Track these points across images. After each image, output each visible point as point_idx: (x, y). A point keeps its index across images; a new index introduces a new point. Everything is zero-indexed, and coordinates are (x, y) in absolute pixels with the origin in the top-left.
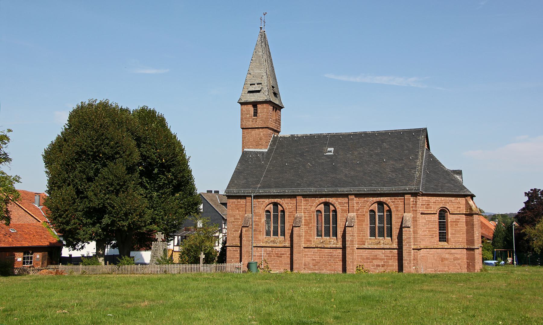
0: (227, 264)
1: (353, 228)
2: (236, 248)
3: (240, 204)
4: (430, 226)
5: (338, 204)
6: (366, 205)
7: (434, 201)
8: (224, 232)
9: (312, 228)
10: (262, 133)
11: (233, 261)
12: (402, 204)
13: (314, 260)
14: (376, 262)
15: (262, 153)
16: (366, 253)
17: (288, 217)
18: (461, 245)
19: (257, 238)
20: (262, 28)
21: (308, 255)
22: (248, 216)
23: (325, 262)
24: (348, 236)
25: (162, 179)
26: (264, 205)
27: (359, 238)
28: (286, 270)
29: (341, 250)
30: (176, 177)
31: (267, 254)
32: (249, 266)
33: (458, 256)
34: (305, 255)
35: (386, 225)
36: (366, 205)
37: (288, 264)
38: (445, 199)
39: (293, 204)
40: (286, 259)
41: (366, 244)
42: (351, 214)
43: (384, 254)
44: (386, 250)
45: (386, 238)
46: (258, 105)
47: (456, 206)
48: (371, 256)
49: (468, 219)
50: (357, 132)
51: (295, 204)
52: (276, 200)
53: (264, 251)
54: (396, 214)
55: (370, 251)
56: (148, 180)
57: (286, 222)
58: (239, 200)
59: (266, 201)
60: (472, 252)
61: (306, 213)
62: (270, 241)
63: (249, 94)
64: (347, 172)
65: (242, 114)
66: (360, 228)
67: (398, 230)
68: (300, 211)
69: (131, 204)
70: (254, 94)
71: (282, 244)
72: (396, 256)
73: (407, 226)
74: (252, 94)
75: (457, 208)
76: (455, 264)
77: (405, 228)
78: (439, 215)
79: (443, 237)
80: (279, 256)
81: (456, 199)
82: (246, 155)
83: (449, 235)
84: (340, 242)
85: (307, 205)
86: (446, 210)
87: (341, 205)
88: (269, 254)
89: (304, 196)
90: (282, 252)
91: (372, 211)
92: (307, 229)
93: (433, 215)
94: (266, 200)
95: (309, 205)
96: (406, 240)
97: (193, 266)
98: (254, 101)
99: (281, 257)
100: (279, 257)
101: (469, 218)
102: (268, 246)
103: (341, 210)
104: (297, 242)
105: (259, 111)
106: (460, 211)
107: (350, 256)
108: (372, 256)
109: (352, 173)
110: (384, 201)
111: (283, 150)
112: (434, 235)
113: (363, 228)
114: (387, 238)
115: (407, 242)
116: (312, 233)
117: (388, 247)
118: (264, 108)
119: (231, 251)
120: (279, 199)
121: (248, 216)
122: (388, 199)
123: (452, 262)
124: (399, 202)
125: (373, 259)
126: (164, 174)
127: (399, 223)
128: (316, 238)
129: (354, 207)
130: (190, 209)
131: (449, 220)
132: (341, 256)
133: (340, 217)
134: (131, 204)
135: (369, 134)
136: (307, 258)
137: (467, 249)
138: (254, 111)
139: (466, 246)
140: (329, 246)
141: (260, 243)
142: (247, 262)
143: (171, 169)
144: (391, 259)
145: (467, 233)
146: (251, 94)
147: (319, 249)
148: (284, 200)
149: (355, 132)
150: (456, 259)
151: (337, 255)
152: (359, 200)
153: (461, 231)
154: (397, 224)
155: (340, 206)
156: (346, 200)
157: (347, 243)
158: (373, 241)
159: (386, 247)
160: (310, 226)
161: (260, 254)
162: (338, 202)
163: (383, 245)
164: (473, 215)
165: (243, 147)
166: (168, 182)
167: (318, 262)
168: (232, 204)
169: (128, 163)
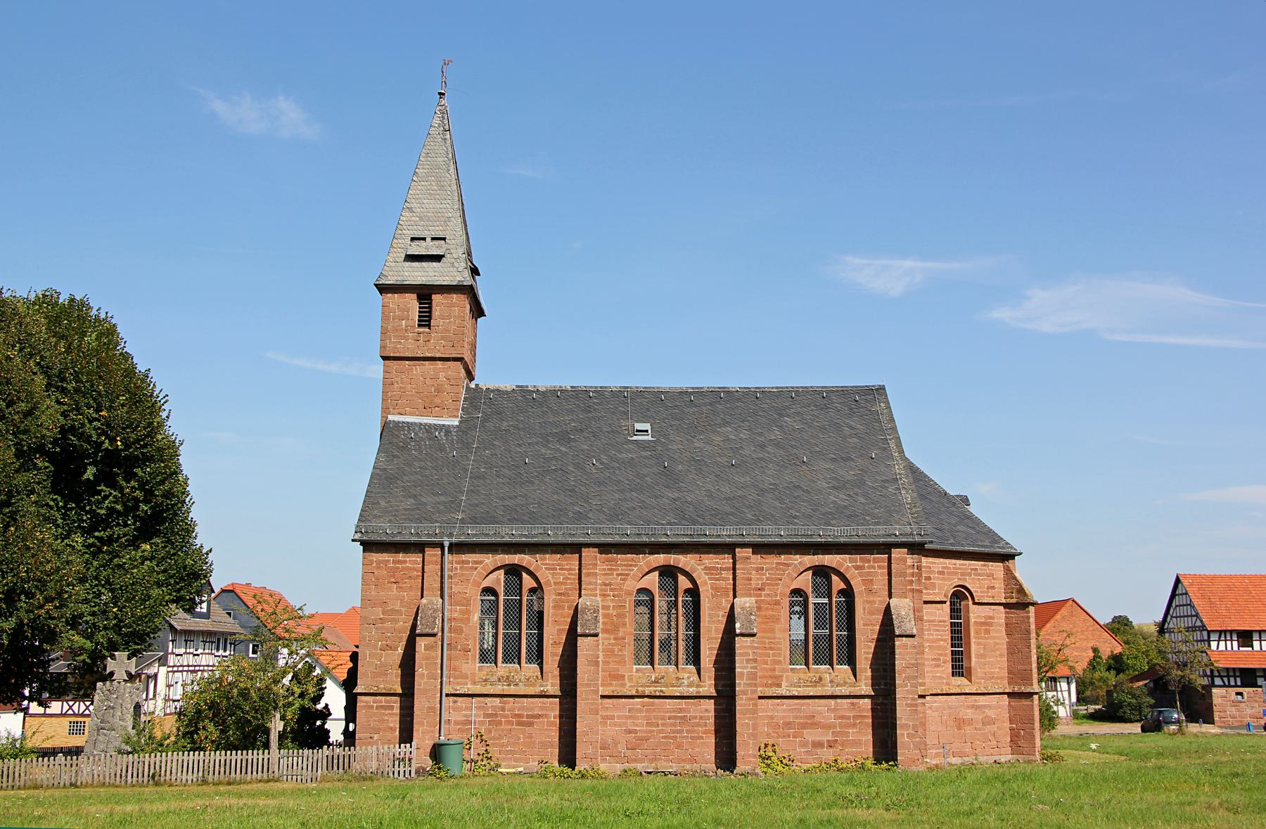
0: (358, 748)
1: (754, 639)
2: (388, 698)
3: (404, 569)
4: (932, 635)
5: (703, 572)
6: (782, 574)
7: (940, 570)
8: (171, 664)
9: (624, 639)
10: (442, 375)
11: (375, 739)
12: (882, 573)
13: (630, 732)
14: (811, 735)
15: (447, 430)
16: (784, 711)
17: (554, 607)
18: (997, 684)
19: (455, 669)
20: (444, 94)
21: (612, 717)
22: (431, 602)
23: (663, 737)
24: (742, 662)
25: (107, 500)
26: (480, 573)
27: (765, 669)
28: (546, 763)
29: (713, 701)
30: (149, 495)
31: (486, 716)
32: (437, 752)
33: (991, 713)
34: (605, 718)
35: (837, 631)
36: (782, 574)
37: (552, 746)
38: (962, 565)
39: (570, 569)
40: (547, 729)
41: (784, 684)
42: (743, 599)
43: (835, 710)
44: (839, 701)
45: (837, 666)
46: (434, 297)
47: (987, 583)
48: (797, 718)
49: (1012, 617)
50: (701, 388)
51: (574, 569)
52: (516, 559)
53: (478, 708)
54: (867, 602)
55: (796, 704)
56: (59, 498)
57: (548, 622)
58: (401, 556)
59: (487, 561)
60: (1025, 703)
61: (609, 595)
62: (495, 678)
63: (408, 264)
64: (709, 486)
65: (385, 318)
66: (767, 641)
67: (873, 645)
68: (590, 589)
69: (29, 564)
70: (424, 264)
71: (534, 685)
72: (865, 716)
73: (908, 633)
74: (417, 263)
75: (988, 588)
76: (986, 734)
77: (900, 638)
78: (951, 605)
79: (959, 666)
80: (526, 722)
81: (985, 565)
82: (397, 433)
83: (973, 659)
84: (710, 680)
85: (613, 574)
86: (966, 592)
87: (712, 574)
88: (493, 718)
89: (605, 548)
90: (532, 709)
91: (797, 592)
92: (613, 641)
93: (938, 606)
94: (484, 557)
95: (618, 575)
96: (904, 672)
97: (251, 755)
98: (424, 283)
99: (531, 724)
100: (523, 725)
101: (1017, 615)
102: (492, 692)
103: (712, 588)
104: (588, 680)
105: (436, 312)
106: (993, 597)
107: (748, 719)
108: (801, 718)
109: (726, 489)
110: (834, 566)
111: (505, 424)
112: (941, 658)
113: (774, 638)
114: (840, 666)
115: (908, 678)
116: (626, 653)
117: (845, 691)
118: (453, 305)
119: (372, 707)
120: (527, 556)
121: (431, 602)
122: (843, 559)
123: (980, 729)
124: (873, 567)
125: (804, 726)
126: (113, 484)
127: (875, 625)
128: (637, 670)
129: (750, 579)
130: (181, 589)
131: (973, 620)
132: (712, 720)
133: (710, 609)
134: (29, 564)
135: (736, 394)
136: (610, 725)
137: (1009, 694)
138: (420, 312)
139: (1007, 686)
140: (676, 691)
141: (467, 684)
142: (429, 744)
143: (138, 471)
144: (854, 725)
145: (1011, 652)
146: (416, 264)
147: (646, 699)
148: (541, 559)
149: (698, 388)
150: (988, 721)
151: (701, 718)
152: (764, 561)
153: (997, 648)
154: (870, 627)
155: (710, 579)
156: (727, 560)
157: (737, 682)
158: (802, 676)
159: (841, 691)
160: (621, 634)
161: (466, 716)
162: (703, 567)
163: (832, 686)
164: (1028, 607)
165: (385, 411)
166: (124, 505)
167: (645, 737)
168: (378, 568)
169: (24, 437)
